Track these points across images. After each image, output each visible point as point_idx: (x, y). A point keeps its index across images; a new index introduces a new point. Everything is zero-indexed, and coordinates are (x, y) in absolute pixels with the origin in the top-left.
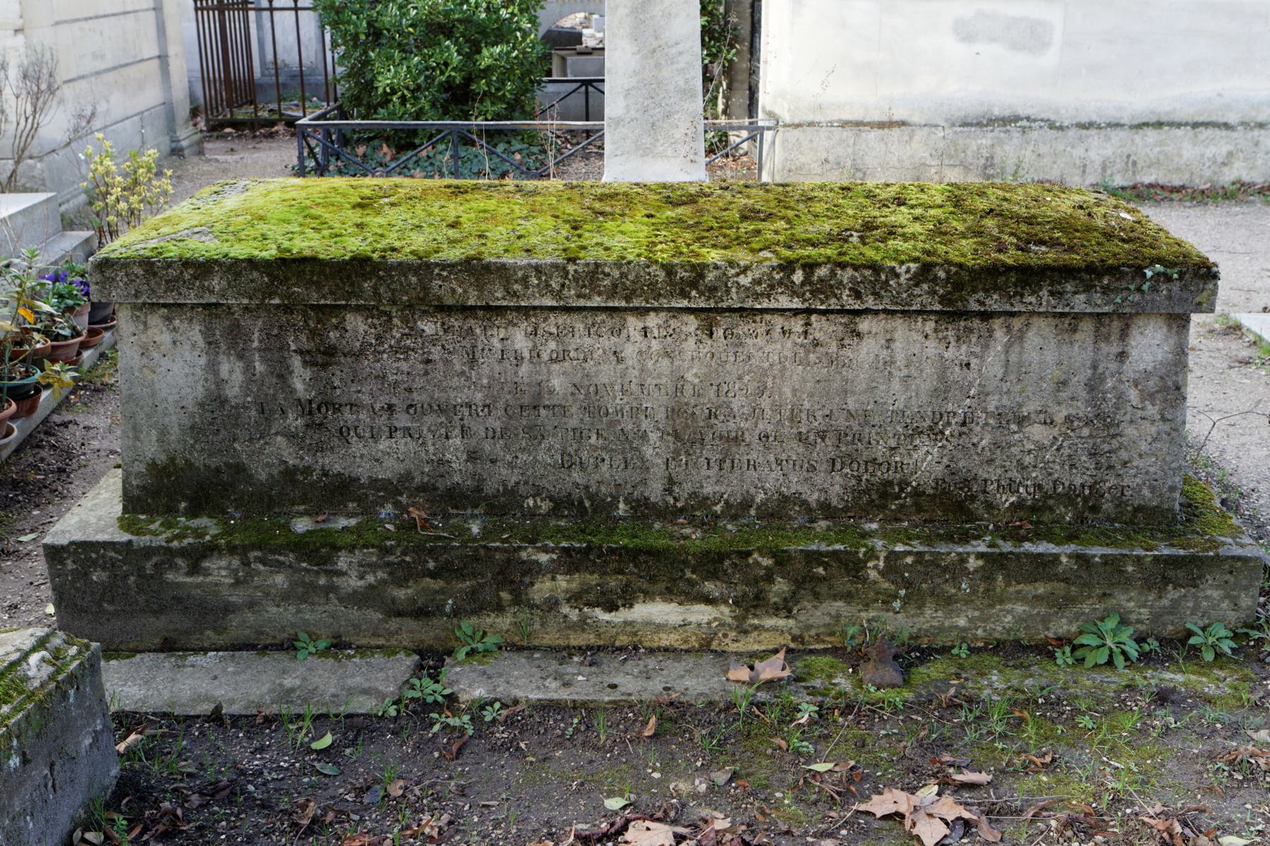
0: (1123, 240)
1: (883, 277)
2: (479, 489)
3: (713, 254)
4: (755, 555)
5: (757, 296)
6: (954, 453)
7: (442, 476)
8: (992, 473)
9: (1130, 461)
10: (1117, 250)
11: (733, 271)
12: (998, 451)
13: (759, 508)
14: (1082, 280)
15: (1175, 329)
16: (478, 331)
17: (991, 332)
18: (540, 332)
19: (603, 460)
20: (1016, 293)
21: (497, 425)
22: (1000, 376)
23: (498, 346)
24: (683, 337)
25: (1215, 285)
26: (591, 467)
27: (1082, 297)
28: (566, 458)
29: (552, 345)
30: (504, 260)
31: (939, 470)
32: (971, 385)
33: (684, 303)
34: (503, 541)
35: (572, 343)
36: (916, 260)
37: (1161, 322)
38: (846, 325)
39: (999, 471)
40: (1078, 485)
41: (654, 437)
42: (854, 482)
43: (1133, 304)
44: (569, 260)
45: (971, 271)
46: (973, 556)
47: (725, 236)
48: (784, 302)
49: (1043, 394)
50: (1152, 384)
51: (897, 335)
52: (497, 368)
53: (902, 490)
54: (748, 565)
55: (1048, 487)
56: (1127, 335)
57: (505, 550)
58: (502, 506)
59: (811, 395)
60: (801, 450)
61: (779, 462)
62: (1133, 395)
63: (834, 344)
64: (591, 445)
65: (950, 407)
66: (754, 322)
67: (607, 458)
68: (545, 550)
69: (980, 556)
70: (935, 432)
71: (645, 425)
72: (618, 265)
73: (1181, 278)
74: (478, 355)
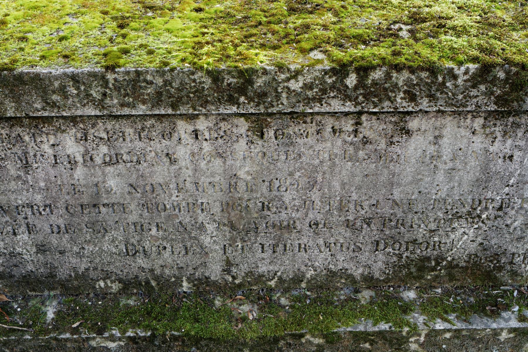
1: (440, 79)
2: (52, 276)
3: (261, 57)
4: (308, 337)
5: (308, 101)
6: (488, 233)
7: (16, 266)
11: (283, 76)
16: (27, 138)
18: (90, 137)
19: (165, 248)
21: (61, 222)
23: (50, 151)
24: (234, 138)
26: (154, 255)
28: (130, 248)
29: (104, 149)
30: (38, 70)
31: (473, 247)
33: (234, 109)
34: (75, 331)
35: (124, 148)
36: (475, 60)
41: (210, 228)
42: (395, 259)
44: (107, 68)
46: (505, 331)
47: (274, 33)
48: (336, 105)
51: (445, 132)
52: (52, 172)
53: (438, 264)
54: (302, 344)
57: (76, 341)
58: (72, 288)
59: (359, 188)
60: (348, 234)
61: (327, 245)
63: (383, 141)
64: (151, 236)
65: (489, 195)
66: (305, 122)
67: (168, 246)
68: (112, 338)
69: (512, 330)
70: (472, 216)
71: (201, 217)
72: (160, 72)
74: (31, 160)
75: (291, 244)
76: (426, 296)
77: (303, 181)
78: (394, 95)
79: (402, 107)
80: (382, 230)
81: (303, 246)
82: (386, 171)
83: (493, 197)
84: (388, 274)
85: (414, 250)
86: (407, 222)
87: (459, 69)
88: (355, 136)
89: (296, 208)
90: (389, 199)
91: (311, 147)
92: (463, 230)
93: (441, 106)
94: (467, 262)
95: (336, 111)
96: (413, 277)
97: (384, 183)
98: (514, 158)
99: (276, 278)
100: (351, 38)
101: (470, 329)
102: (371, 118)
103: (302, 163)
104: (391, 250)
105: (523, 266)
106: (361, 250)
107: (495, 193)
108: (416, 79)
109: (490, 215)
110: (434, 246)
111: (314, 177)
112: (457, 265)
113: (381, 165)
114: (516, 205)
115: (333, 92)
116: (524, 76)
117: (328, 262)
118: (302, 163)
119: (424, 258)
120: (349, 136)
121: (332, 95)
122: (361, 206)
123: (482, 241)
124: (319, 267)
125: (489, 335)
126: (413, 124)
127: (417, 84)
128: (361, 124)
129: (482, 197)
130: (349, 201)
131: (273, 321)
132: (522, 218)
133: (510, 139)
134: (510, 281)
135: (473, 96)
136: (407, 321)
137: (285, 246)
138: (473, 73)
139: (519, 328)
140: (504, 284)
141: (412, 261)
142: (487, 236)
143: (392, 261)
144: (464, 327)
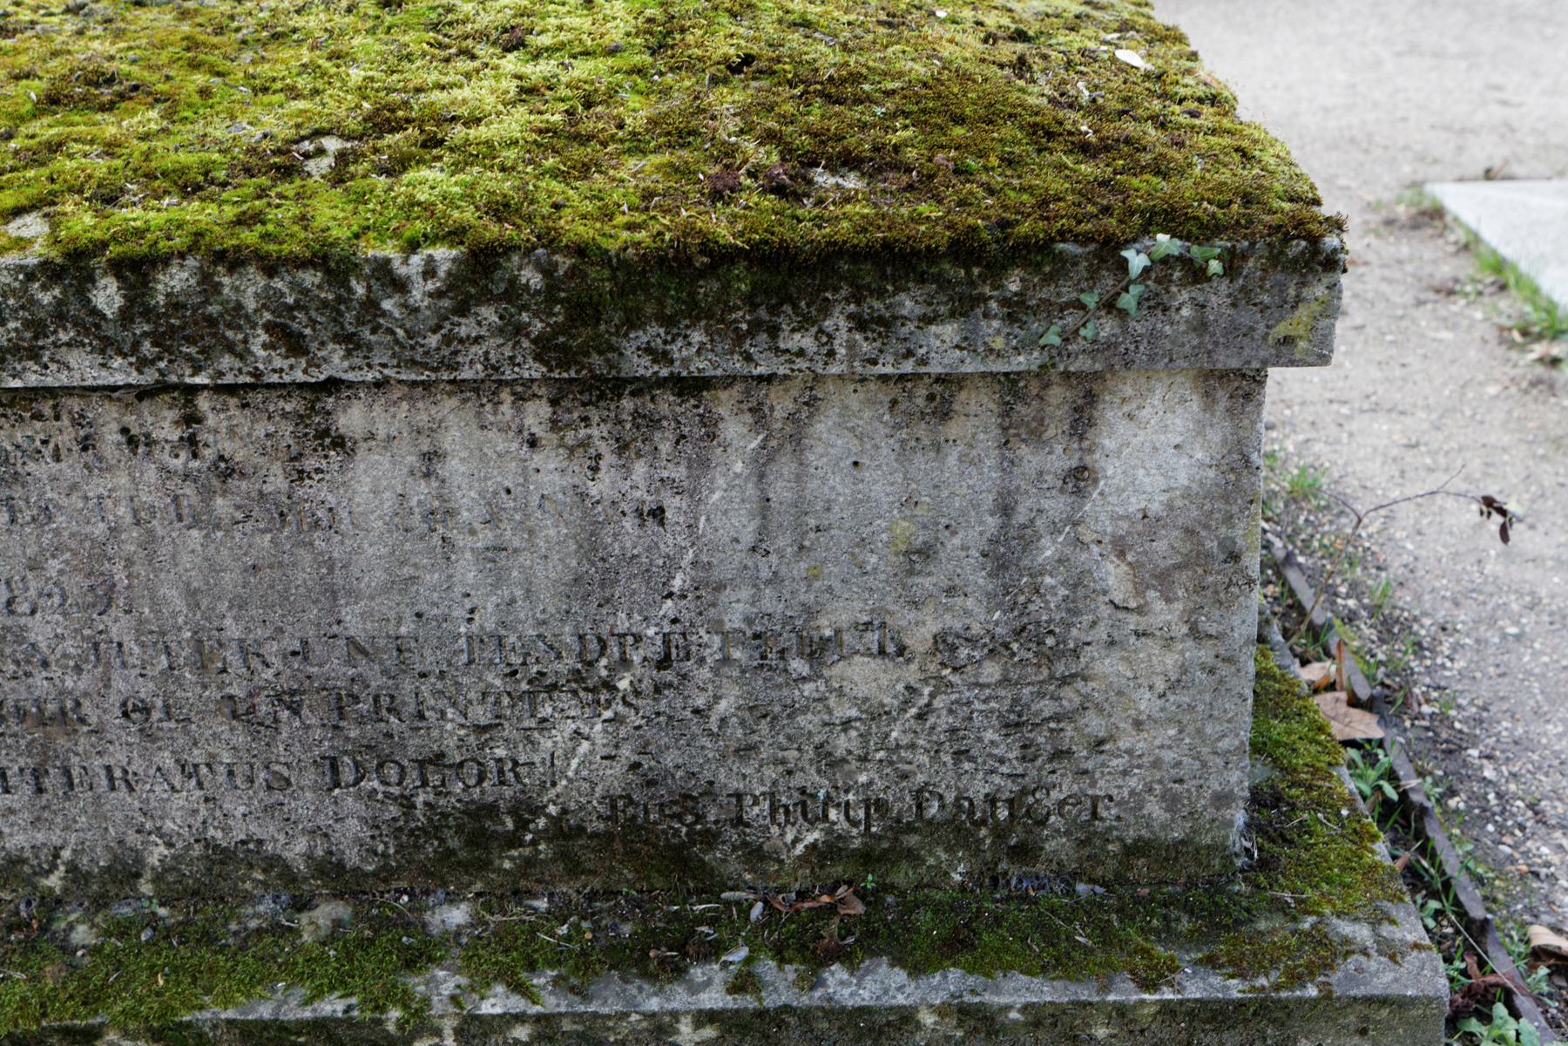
0: (1085, 149)
1: (360, 290)
6: (649, 733)
8: (756, 778)
9: (1112, 738)
10: (1057, 185)
12: (764, 726)
13: (157, 879)
14: (943, 283)
15: (1223, 402)
17: (710, 427)
20: (756, 326)
22: (748, 538)
25: (1332, 287)
27: (949, 331)
31: (614, 776)
32: (671, 565)
36: (456, 235)
37: (1184, 387)
38: (300, 419)
39: (771, 773)
40: (979, 800)
42: (394, 810)
43: (1098, 348)
45: (617, 265)
49: (871, 581)
50: (1164, 547)
55: (903, 805)
56: (1091, 423)
60: (240, 739)
61: (189, 771)
62: (1114, 577)
63: (277, 468)
65: (622, 623)
66: (38, 416)
73: (1231, 271)
75: (84, 768)
76: (498, 918)
77: (76, 584)
78: (240, 336)
79: (274, 371)
80: (336, 727)
81: (118, 773)
82: (305, 557)
83: (634, 630)
84: (385, 855)
85: (443, 784)
86: (404, 703)
87: (405, 262)
88: (195, 456)
89: (71, 663)
90: (335, 636)
91: (74, 487)
92: (574, 726)
93: (384, 366)
94: (608, 818)
95: (89, 383)
96: (459, 863)
97: (310, 591)
98: (668, 514)
99: (62, 868)
100: (156, 178)
101: (581, 1015)
102: (225, 403)
103: (57, 532)
104: (375, 784)
105: (775, 830)
106: (289, 783)
107: (637, 617)
108: (292, 289)
109: (640, 681)
110: (501, 772)
111: (102, 574)
112: (580, 830)
113: (288, 538)
114: (708, 651)
115: (65, 329)
116: (594, 280)
117: (200, 819)
118: (57, 532)
119: (478, 809)
120: (177, 456)
121: (64, 337)
122: (258, 655)
123: (634, 758)
124: (179, 834)
125: (640, 1032)
126: (351, 418)
127: (297, 306)
128: (199, 421)
129: (604, 630)
130: (221, 645)
131: (23, 989)
132: (736, 691)
133: (642, 462)
134: (748, 877)
135: (468, 337)
136: (405, 991)
137: (67, 772)
138: (449, 273)
139: (723, 1011)
140: (730, 883)
141: (444, 815)
142: (647, 744)
143: (387, 816)
144: (563, 1009)
